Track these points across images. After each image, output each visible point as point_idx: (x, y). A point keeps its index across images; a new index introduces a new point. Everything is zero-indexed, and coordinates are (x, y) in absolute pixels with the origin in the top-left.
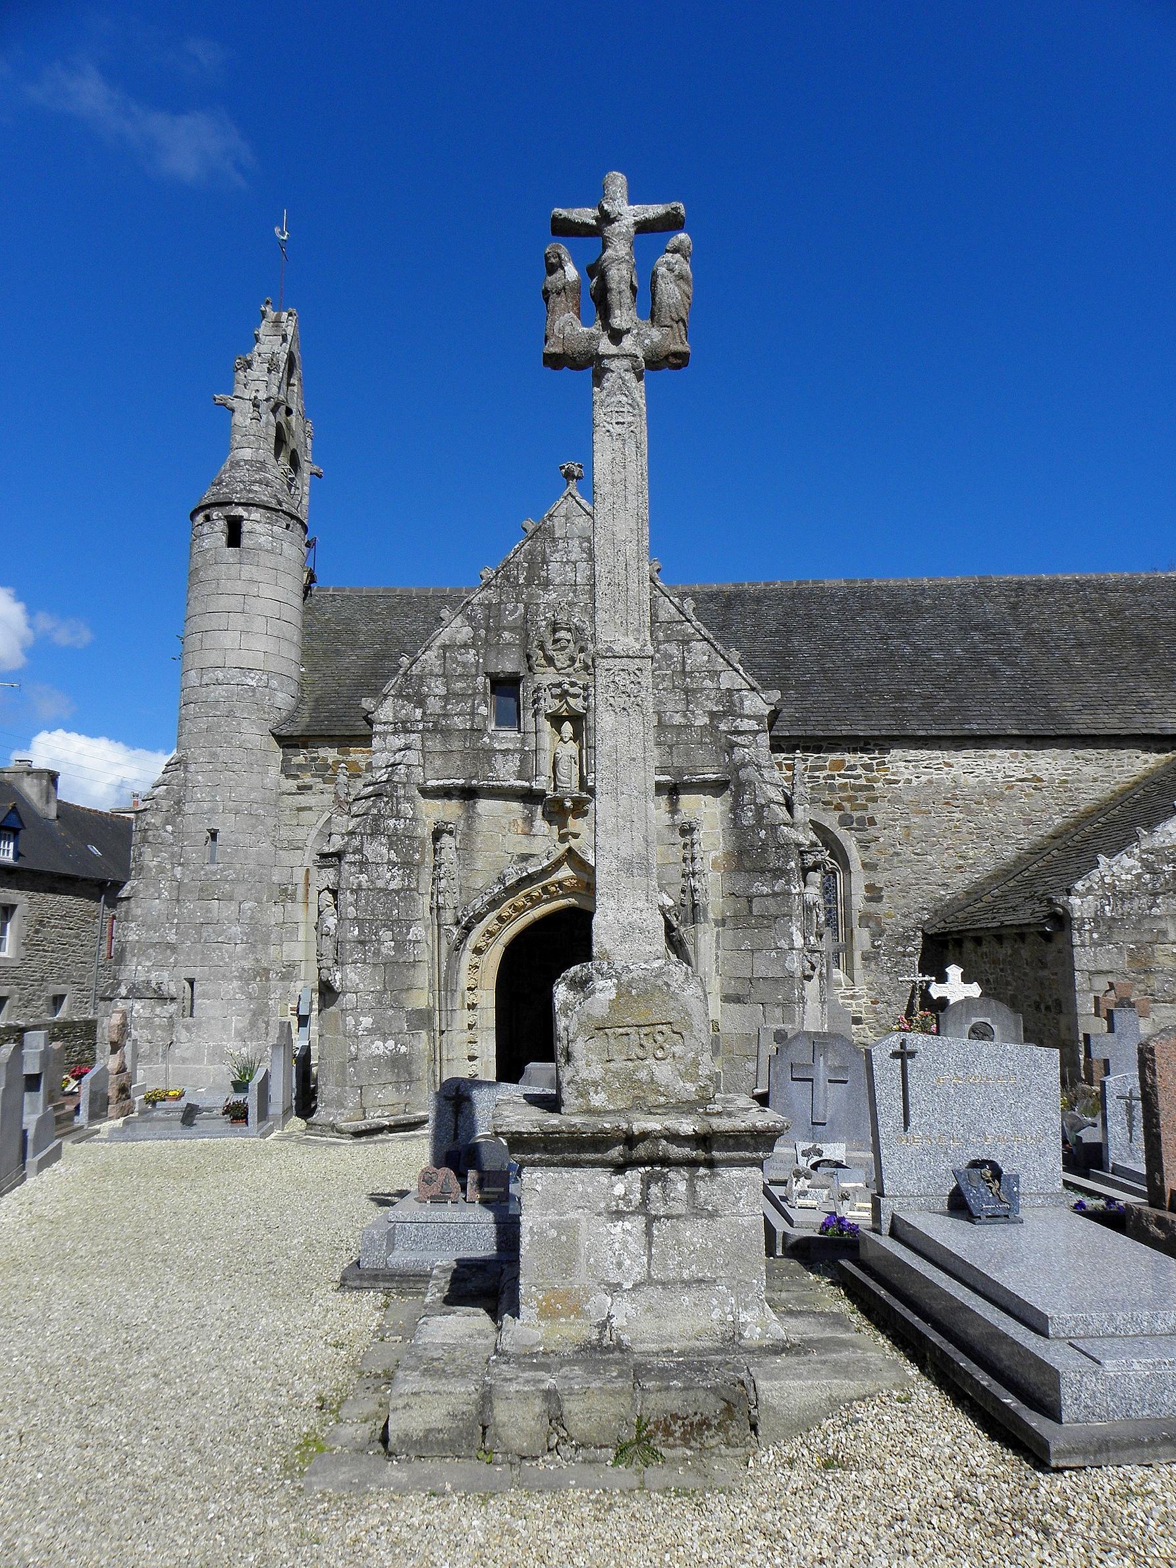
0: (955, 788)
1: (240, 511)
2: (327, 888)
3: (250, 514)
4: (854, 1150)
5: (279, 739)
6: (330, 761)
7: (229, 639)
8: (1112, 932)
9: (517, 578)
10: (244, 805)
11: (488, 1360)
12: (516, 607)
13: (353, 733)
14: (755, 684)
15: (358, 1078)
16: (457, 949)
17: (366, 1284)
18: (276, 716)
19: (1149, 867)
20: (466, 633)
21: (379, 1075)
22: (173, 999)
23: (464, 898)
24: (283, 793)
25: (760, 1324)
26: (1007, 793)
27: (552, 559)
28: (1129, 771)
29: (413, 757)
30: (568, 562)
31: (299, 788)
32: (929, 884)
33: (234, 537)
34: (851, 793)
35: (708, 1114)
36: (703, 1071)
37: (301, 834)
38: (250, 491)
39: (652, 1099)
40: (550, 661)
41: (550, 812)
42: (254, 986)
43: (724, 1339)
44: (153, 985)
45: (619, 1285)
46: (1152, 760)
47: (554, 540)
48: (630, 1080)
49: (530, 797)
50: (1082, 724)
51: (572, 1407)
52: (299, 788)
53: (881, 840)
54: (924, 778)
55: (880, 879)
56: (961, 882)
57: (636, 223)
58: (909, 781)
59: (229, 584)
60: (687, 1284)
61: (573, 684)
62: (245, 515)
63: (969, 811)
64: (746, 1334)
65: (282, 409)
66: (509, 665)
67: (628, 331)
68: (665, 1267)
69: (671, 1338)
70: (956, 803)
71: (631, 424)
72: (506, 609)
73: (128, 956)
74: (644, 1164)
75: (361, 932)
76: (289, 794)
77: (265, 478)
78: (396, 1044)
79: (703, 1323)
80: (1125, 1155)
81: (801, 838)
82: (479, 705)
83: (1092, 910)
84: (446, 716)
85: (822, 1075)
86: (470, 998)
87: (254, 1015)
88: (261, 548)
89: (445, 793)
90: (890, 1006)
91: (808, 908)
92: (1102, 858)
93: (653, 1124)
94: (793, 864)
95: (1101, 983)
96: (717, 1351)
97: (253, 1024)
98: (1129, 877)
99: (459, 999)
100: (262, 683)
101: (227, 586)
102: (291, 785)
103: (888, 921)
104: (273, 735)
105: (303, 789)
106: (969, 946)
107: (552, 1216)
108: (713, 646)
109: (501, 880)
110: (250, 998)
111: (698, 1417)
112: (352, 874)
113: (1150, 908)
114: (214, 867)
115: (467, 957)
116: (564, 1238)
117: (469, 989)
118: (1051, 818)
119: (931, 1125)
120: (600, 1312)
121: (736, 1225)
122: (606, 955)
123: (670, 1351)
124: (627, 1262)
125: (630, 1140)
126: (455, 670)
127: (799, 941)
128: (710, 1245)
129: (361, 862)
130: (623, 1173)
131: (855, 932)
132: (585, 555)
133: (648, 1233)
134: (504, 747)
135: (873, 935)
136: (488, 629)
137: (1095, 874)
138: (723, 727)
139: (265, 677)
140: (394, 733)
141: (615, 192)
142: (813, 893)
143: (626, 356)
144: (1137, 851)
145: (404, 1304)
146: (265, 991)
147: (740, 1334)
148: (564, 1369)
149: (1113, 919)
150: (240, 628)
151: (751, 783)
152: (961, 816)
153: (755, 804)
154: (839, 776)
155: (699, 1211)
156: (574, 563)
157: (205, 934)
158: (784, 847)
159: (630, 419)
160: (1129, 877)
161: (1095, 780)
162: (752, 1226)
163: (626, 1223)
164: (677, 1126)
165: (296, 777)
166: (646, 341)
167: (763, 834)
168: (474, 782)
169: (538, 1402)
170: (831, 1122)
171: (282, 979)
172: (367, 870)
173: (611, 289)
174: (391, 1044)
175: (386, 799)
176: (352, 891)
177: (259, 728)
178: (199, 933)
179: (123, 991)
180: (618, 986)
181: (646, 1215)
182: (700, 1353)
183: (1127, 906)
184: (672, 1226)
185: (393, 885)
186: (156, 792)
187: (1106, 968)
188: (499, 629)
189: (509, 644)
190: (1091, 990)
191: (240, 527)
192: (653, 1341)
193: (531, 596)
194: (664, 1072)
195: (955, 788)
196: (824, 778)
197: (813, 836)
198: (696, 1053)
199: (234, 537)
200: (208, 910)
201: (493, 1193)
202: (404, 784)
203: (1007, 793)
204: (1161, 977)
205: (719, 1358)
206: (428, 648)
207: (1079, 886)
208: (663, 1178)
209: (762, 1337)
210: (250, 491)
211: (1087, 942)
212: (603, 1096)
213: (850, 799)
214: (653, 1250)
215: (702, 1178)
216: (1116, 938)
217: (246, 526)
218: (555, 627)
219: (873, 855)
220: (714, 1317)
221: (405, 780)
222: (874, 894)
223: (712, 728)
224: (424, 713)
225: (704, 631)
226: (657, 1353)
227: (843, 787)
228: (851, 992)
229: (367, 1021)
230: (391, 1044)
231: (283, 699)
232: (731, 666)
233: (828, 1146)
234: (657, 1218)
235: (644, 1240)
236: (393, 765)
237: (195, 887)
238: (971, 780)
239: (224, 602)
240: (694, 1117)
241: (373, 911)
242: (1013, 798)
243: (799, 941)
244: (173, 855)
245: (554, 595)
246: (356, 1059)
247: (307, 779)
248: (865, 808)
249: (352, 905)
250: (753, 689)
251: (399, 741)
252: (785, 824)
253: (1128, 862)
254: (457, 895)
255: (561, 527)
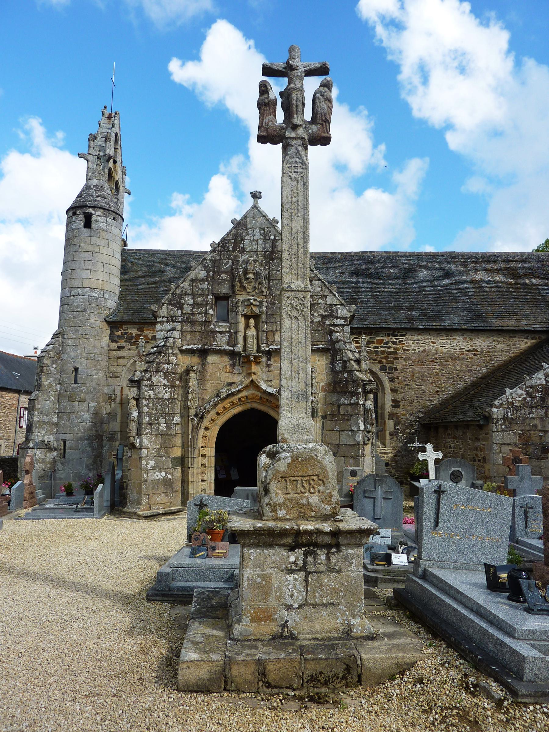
0: (436, 354)
1: (91, 211)
2: (134, 398)
3: (95, 212)
4: (394, 532)
5: (108, 323)
6: (134, 335)
7: (84, 274)
8: (511, 425)
9: (228, 247)
10: (91, 355)
11: (227, 643)
12: (228, 262)
13: (145, 321)
14: (343, 302)
15: (148, 490)
16: (197, 428)
17: (158, 598)
18: (107, 312)
19: (529, 394)
20: (203, 274)
21: (157, 489)
22: (55, 449)
23: (200, 403)
24: (111, 350)
25: (362, 624)
26: (461, 356)
27: (246, 238)
28: (518, 347)
29: (176, 334)
30: (254, 240)
31: (118, 347)
32: (422, 400)
33: (88, 223)
34: (386, 355)
35: (336, 521)
36: (334, 500)
37: (119, 370)
38: (96, 201)
39: (308, 513)
40: (245, 288)
41: (243, 362)
42: (95, 444)
43: (343, 633)
44: (46, 442)
45: (292, 606)
46: (529, 343)
47: (247, 229)
48: (297, 504)
49: (232, 354)
50: (497, 324)
51: (271, 667)
52: (118, 347)
53: (400, 378)
54: (422, 349)
55: (399, 397)
56: (438, 399)
57: (305, 71)
58: (414, 350)
59: (85, 247)
60: (325, 605)
61: (255, 300)
62: (93, 212)
63: (441, 364)
64: (354, 630)
65: (112, 160)
66: (224, 290)
67: (301, 125)
68: (314, 597)
69: (317, 632)
70: (437, 361)
71: (301, 173)
72: (223, 263)
73: (34, 428)
74: (304, 547)
75: (150, 419)
76: (113, 350)
77: (103, 194)
78: (166, 474)
79: (333, 625)
80: (523, 535)
81: (364, 377)
82: (209, 309)
83: (502, 414)
84: (193, 314)
85: (379, 496)
86: (202, 452)
87: (95, 458)
88: (100, 229)
89: (191, 352)
90: (402, 458)
91: (367, 411)
92: (508, 390)
93: (309, 526)
94: (360, 390)
95: (506, 449)
96: (340, 639)
97: (95, 462)
98: (520, 399)
99: (197, 452)
100: (100, 296)
101: (85, 247)
102: (114, 345)
103: (403, 417)
104: (106, 321)
105: (120, 348)
106: (441, 430)
107: (258, 571)
108: (323, 282)
109: (218, 396)
110: (93, 449)
111: (333, 673)
112: (146, 391)
113: (529, 414)
114: (75, 385)
115: (202, 432)
116: (264, 583)
117: (202, 447)
118: (481, 369)
119: (448, 528)
120: (282, 619)
121: (350, 576)
122: (285, 440)
123: (317, 639)
124: (296, 595)
125: (298, 533)
126: (197, 292)
127: (362, 427)
128: (337, 586)
129: (151, 385)
130: (294, 551)
131: (387, 422)
132: (262, 237)
133: (306, 580)
134: (221, 330)
135: (395, 424)
136: (214, 272)
137: (504, 397)
138: (327, 322)
139: (102, 293)
140: (167, 322)
141: (294, 55)
142: (370, 404)
143: (299, 138)
144: (524, 387)
145: (181, 610)
146: (101, 447)
147: (351, 630)
148: (265, 649)
149: (512, 419)
150: (90, 268)
151: (341, 350)
152: (439, 367)
153: (342, 360)
154: (381, 347)
155: (331, 570)
156: (257, 240)
157: (71, 418)
158: (357, 382)
159: (302, 170)
160: (520, 399)
161: (502, 351)
162: (359, 577)
163: (296, 575)
164: (322, 528)
165: (117, 342)
166: (310, 131)
167: (346, 375)
168: (206, 347)
169: (253, 665)
170: (384, 518)
171: (109, 440)
172: (153, 389)
173: (293, 104)
174: (163, 474)
175: (163, 354)
176: (146, 399)
177: (99, 317)
178: (68, 417)
179: (31, 445)
180: (292, 457)
181: (305, 571)
182: (332, 639)
183: (518, 413)
184: (318, 577)
185: (166, 396)
186: (48, 348)
187: (508, 442)
188: (219, 273)
189: (225, 280)
190: (501, 452)
191: (91, 218)
192: (308, 634)
193: (235, 256)
194: (314, 500)
195: (436, 354)
196: (373, 348)
197: (370, 377)
198: (331, 490)
199: (88, 223)
200: (73, 406)
201: (221, 553)
202: (172, 348)
203: (461, 356)
204: (533, 447)
205: (340, 642)
206: (184, 281)
207: (496, 402)
208: (313, 553)
209: (362, 632)
210: (96, 201)
211: (500, 430)
212: (284, 511)
213: (386, 358)
214: (309, 589)
215: (333, 553)
216: (513, 428)
217: (94, 218)
218: (246, 272)
219: (396, 385)
220: (338, 621)
221: (172, 345)
222: (396, 404)
223: (322, 323)
224: (182, 313)
225: (320, 276)
226: (310, 640)
227: (382, 352)
228: (384, 451)
229: (152, 463)
230: (163, 474)
231: (112, 303)
232: (332, 293)
233: (383, 530)
234: (311, 573)
235: (304, 583)
236: (167, 338)
237: (67, 395)
238: (444, 350)
239: (83, 255)
240: (329, 523)
241: (156, 409)
242: (464, 359)
243: (362, 427)
244: (56, 379)
245: (247, 256)
246: (146, 481)
247: (123, 343)
248: (392, 362)
249: (146, 406)
250: (342, 304)
251: (168, 326)
252: (357, 371)
253: (520, 392)
254: (197, 402)
255: (250, 223)
